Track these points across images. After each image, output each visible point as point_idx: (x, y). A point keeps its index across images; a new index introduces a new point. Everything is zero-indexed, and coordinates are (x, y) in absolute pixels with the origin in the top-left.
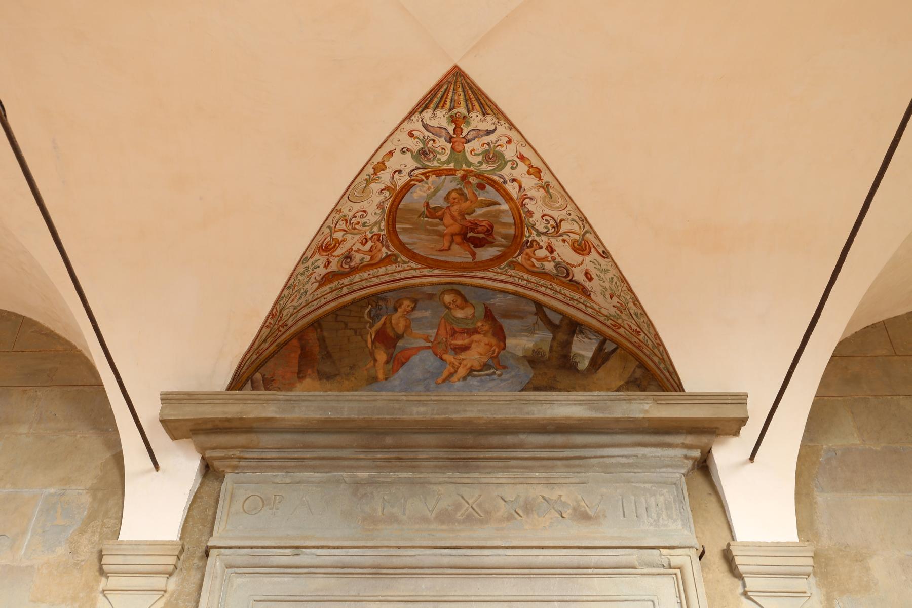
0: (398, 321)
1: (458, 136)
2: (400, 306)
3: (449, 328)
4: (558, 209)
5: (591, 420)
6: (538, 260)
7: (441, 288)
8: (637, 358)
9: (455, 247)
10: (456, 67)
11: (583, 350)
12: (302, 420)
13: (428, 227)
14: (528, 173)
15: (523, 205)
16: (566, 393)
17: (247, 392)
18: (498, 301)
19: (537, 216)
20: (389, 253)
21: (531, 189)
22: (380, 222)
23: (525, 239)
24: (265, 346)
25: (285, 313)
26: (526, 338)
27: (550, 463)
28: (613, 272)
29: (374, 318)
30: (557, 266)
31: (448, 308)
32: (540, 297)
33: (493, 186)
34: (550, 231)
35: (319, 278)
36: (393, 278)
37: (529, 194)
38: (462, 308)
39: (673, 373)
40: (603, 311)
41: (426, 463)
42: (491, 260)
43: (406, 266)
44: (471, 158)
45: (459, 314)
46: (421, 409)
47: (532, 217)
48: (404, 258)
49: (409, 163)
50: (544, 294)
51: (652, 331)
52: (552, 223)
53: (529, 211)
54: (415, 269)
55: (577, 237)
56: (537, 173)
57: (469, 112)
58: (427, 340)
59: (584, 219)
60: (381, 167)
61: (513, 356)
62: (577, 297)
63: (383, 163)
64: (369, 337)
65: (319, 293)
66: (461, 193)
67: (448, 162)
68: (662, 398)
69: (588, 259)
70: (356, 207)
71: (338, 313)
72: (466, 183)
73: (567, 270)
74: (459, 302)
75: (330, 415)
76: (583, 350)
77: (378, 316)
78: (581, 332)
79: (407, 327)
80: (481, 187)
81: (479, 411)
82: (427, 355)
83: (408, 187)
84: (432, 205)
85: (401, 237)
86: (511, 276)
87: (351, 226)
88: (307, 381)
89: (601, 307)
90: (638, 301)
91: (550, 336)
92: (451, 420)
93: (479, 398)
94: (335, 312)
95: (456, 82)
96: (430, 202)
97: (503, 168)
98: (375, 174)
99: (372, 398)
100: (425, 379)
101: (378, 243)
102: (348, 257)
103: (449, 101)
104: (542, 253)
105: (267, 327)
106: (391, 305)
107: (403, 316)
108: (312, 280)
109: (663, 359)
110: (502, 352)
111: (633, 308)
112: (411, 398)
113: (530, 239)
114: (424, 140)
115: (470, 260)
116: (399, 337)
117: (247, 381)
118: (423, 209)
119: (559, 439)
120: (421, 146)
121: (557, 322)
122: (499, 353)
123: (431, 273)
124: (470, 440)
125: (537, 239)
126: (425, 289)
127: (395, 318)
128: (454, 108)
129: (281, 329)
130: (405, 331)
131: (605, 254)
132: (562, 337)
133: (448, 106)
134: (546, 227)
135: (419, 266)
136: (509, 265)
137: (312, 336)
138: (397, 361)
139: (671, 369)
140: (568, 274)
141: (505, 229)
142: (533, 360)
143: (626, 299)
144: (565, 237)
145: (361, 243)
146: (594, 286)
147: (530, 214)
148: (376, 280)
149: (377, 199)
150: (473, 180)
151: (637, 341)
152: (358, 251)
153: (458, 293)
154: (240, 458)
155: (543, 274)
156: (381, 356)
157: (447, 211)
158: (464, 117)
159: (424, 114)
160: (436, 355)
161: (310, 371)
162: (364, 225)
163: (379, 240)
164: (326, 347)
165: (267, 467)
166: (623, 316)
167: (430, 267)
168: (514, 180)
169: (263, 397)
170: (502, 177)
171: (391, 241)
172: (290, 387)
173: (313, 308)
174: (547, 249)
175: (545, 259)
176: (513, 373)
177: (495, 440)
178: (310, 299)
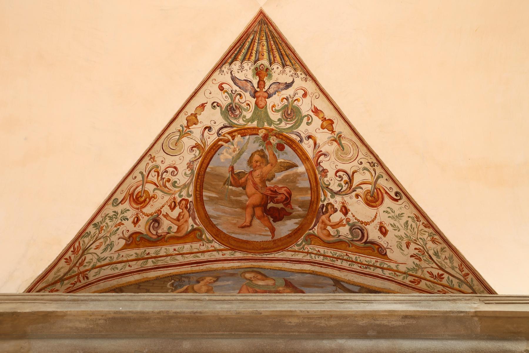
1: (261, 90)
4: (351, 160)
6: (333, 226)
7: (243, 270)
10: (261, 13)
14: (322, 127)
15: (318, 164)
19: (331, 174)
20: (195, 226)
21: (325, 144)
23: (321, 203)
32: (336, 273)
33: (291, 146)
34: (344, 188)
35: (127, 235)
37: (324, 150)
42: (289, 236)
43: (209, 245)
47: (326, 176)
50: (340, 269)
52: (345, 178)
55: (369, 187)
57: (271, 64)
60: (193, 120)
63: (195, 115)
66: (264, 156)
67: (252, 120)
69: (382, 208)
70: (169, 160)
71: (141, 284)
72: (267, 144)
73: (362, 230)
80: (280, 147)
83: (216, 147)
84: (236, 171)
85: (207, 207)
86: (308, 253)
95: (261, 31)
96: (235, 166)
97: (299, 125)
98: (188, 127)
101: (185, 211)
103: (254, 52)
104: (337, 217)
113: (325, 203)
114: (232, 95)
115: (269, 238)
118: (228, 175)
120: (229, 101)
123: (232, 257)
125: (332, 201)
128: (258, 60)
133: (253, 58)
134: (340, 185)
135: (222, 247)
136: (306, 240)
144: (359, 191)
146: (389, 242)
147: (325, 172)
148: (180, 259)
149: (189, 157)
155: (339, 243)
158: (267, 69)
159: (233, 65)
166: (423, 264)
167: (232, 249)
168: (309, 137)
170: (299, 135)
171: (198, 211)
173: (117, 272)
174: (341, 211)
175: (339, 224)
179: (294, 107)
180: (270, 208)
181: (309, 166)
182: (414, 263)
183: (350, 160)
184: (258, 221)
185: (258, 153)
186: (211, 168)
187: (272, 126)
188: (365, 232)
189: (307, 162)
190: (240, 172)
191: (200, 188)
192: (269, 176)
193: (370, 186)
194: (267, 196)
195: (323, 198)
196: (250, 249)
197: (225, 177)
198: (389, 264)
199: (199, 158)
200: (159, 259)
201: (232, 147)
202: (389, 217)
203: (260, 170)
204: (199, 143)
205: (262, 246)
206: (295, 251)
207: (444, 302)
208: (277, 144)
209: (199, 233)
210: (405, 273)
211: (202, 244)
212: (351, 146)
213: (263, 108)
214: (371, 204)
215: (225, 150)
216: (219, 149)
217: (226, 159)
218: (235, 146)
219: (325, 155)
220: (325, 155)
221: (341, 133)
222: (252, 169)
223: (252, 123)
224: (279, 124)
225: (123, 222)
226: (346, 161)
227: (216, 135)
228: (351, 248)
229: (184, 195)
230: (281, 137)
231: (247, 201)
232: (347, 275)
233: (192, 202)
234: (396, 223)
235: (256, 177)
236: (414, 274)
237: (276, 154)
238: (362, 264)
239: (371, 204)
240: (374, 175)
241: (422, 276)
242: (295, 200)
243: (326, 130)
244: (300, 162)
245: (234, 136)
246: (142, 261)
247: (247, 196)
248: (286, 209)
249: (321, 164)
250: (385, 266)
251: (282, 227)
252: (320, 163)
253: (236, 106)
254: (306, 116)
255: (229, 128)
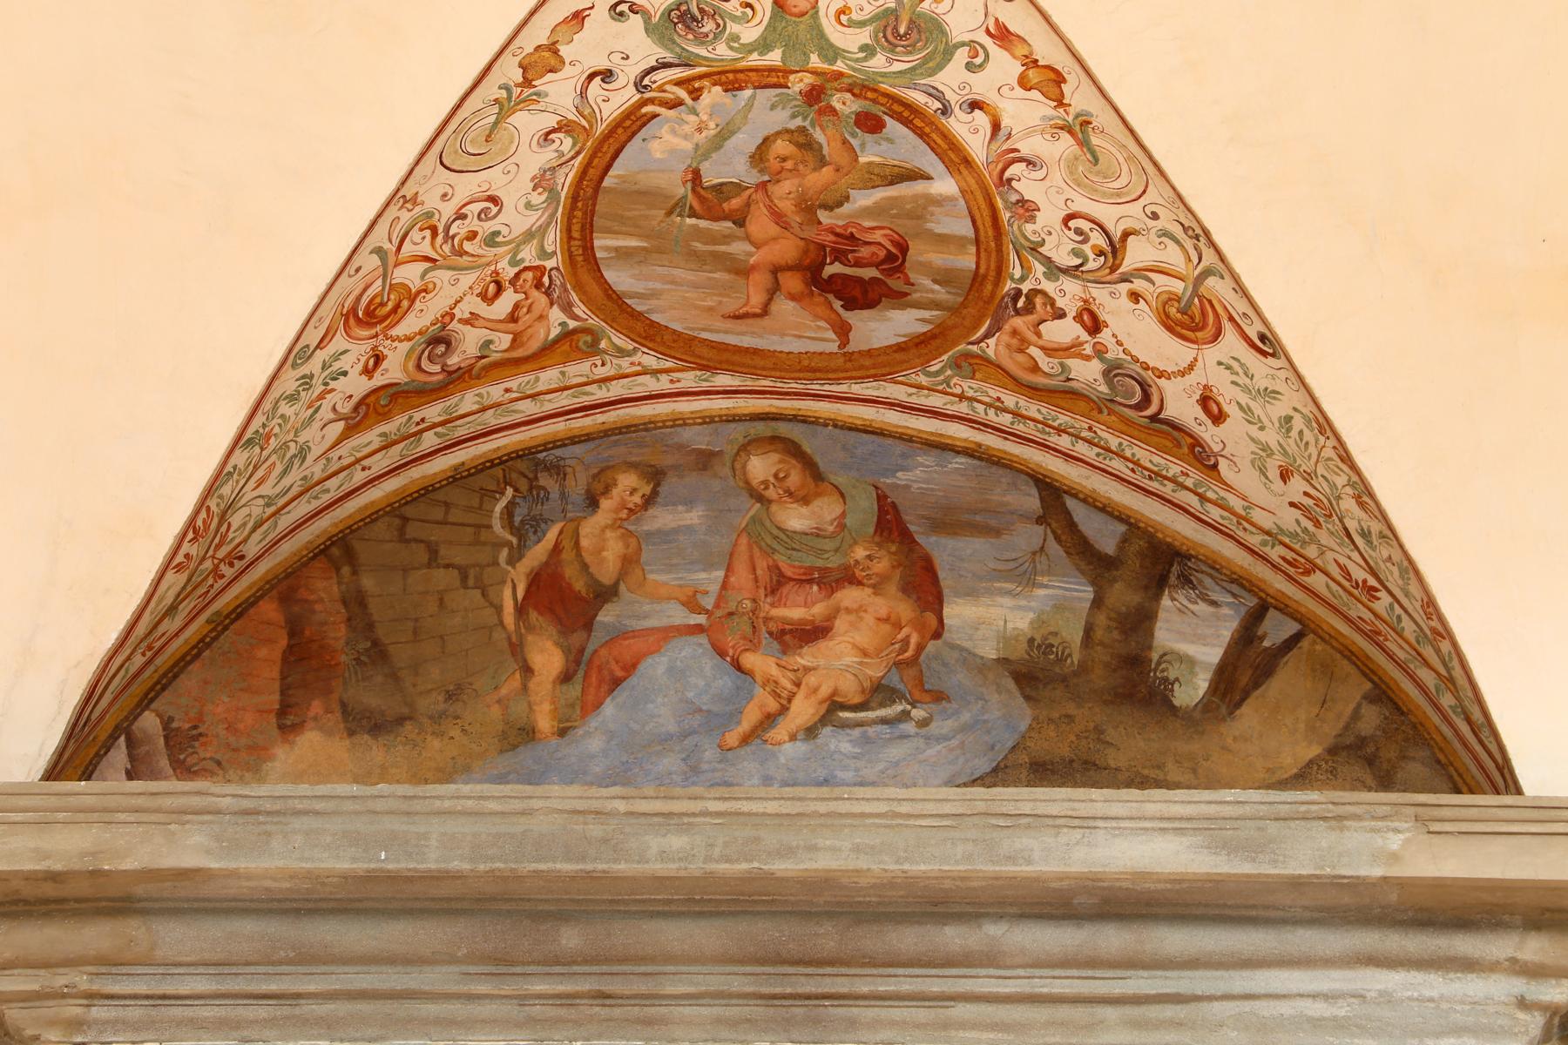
0: (600, 541)
2: (607, 490)
3: (762, 565)
4: (1118, 198)
5: (1217, 882)
6: (1049, 351)
7: (738, 432)
8: (1366, 669)
9: (784, 307)
11: (1192, 637)
12: (293, 876)
13: (698, 246)
14: (1023, 83)
15: (1005, 183)
16: (1134, 793)
17: (112, 785)
18: (919, 477)
19: (1049, 217)
20: (572, 324)
21: (1030, 132)
22: (543, 230)
23: (1009, 286)
24: (171, 626)
25: (236, 520)
26: (1007, 601)
27: (1079, 1013)
28: (1291, 399)
29: (525, 530)
30: (1112, 371)
31: (760, 498)
33: (906, 122)
34: (1091, 265)
35: (345, 408)
36: (586, 400)
37: (1025, 148)
38: (805, 501)
39: (1484, 728)
40: (1258, 516)
41: (687, 1011)
42: (900, 348)
43: (625, 364)
44: (837, 36)
45: (796, 519)
46: (675, 837)
47: (1032, 219)
48: (620, 341)
49: (634, 46)
50: (1068, 457)
51: (1414, 588)
52: (1097, 239)
53: (1022, 202)
54: (655, 373)
55: (1178, 286)
56: (1052, 83)
58: (692, 605)
59: (1200, 235)
60: (547, 59)
61: (968, 658)
62: (1174, 469)
63: (552, 48)
64: (507, 593)
65: (346, 451)
66: (804, 142)
67: (763, 45)
68: (1437, 812)
69: (1212, 354)
70: (467, 186)
71: (409, 511)
72: (820, 112)
74: (795, 478)
75: (384, 860)
76: (1192, 637)
77: (537, 524)
78: (1186, 581)
79: (629, 562)
80: (870, 123)
81: (857, 849)
82: (692, 651)
83: (632, 123)
84: (710, 177)
85: (610, 275)
87: (449, 243)
88: (310, 740)
89: (1250, 505)
90: (1372, 495)
91: (1087, 593)
92: (770, 877)
93: (857, 808)
94: (398, 511)
97: (940, 67)
98: (527, 82)
99: (517, 805)
100: (685, 735)
101: (536, 294)
102: (440, 340)
105: (179, 568)
106: (577, 486)
107: (617, 524)
108: (325, 413)
109: (1451, 680)
110: (932, 646)
111: (1355, 517)
112: (643, 806)
115: (833, 347)
116: (605, 594)
117: (113, 737)
119: (1112, 938)
121: (1108, 546)
122: (920, 648)
123: (705, 385)
124: (827, 938)
125: (1048, 286)
126: (687, 435)
127: (590, 528)
129: (224, 569)
130: (623, 574)
131: (1267, 344)
132: (1123, 595)
135: (669, 364)
136: (956, 364)
137: (325, 591)
138: (597, 675)
139: (1477, 715)
140: (1147, 398)
141: (947, 252)
142: (1031, 672)
143: (1333, 486)
144: (1139, 285)
145: (483, 296)
147: (1027, 209)
148: (528, 408)
149: (535, 160)
150: (844, 104)
151: (1368, 616)
152: (472, 320)
153: (793, 450)
154: (92, 997)
155: (1066, 395)
156: (547, 657)
157: (759, 196)
160: (722, 653)
161: (317, 707)
162: (492, 240)
163: (538, 285)
164: (371, 626)
165: (180, 1023)
168: (975, 105)
169: (168, 802)
171: (579, 287)
172: (249, 759)
173: (325, 499)
174: (1078, 318)
175: (1072, 349)
176: (966, 717)
177: (907, 939)
178: (317, 471)
179: (919, 15)
180: (831, 276)
181: (972, 182)
182: (1298, 522)
183: (1118, 195)
184: (792, 304)
185: (786, 136)
186: (618, 177)
187: (839, 63)
188: (1154, 390)
189: (965, 172)
190: (722, 184)
191: (583, 229)
192: (829, 198)
193: (1182, 284)
194: (823, 247)
195: (1017, 273)
196: (764, 369)
197: (667, 197)
198: (1222, 493)
199: (573, 158)
200: (458, 423)
201: (692, 118)
202: (1233, 382)
203: (796, 181)
204: (571, 117)
205: (806, 363)
206: (920, 387)
207: (1309, 824)
208: (858, 115)
209: (589, 338)
210: (1268, 533)
211: (599, 363)
212: (1121, 160)
213: (803, 14)
214: (1178, 329)
215: (666, 128)
216: (644, 125)
217: (673, 151)
218: (705, 118)
219: (1029, 163)
220: (1029, 163)
221: (1089, 114)
222: (766, 178)
223: (761, 54)
224: (865, 59)
225: (333, 384)
226: (1104, 194)
227: (631, 89)
228: (1104, 417)
229: (528, 257)
230: (869, 94)
231: (751, 255)
232: (1087, 478)
233: (557, 269)
234: (1252, 404)
235: (781, 198)
236: (1297, 547)
237: (855, 142)
238: (1137, 463)
239: (1178, 329)
240: (1195, 261)
241: (1318, 561)
242: (921, 264)
243: (1035, 94)
244: (941, 167)
245: (700, 89)
246: (402, 445)
247: (752, 243)
248: (890, 282)
249: (1014, 183)
250: (1210, 495)
251: (873, 325)
252: (1009, 180)
253: (701, 10)
254: (963, 44)
255: (678, 70)
